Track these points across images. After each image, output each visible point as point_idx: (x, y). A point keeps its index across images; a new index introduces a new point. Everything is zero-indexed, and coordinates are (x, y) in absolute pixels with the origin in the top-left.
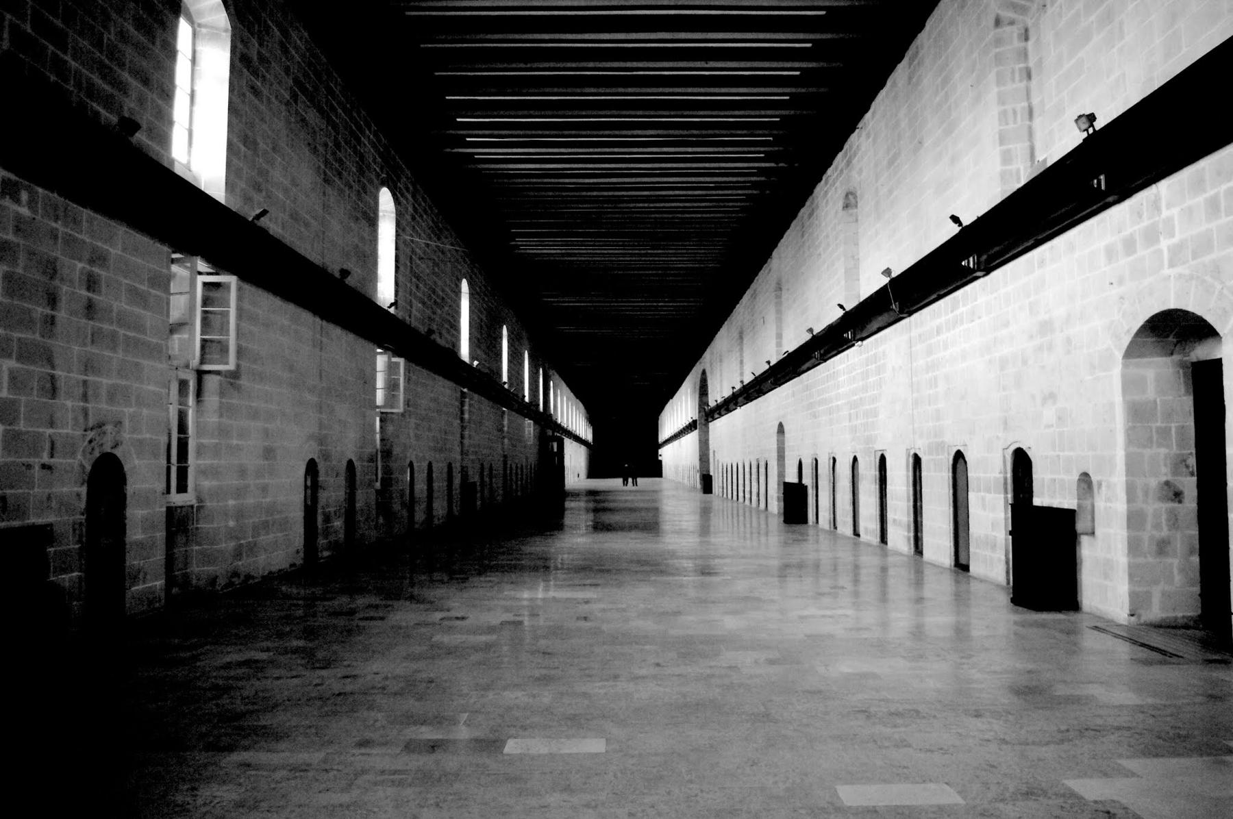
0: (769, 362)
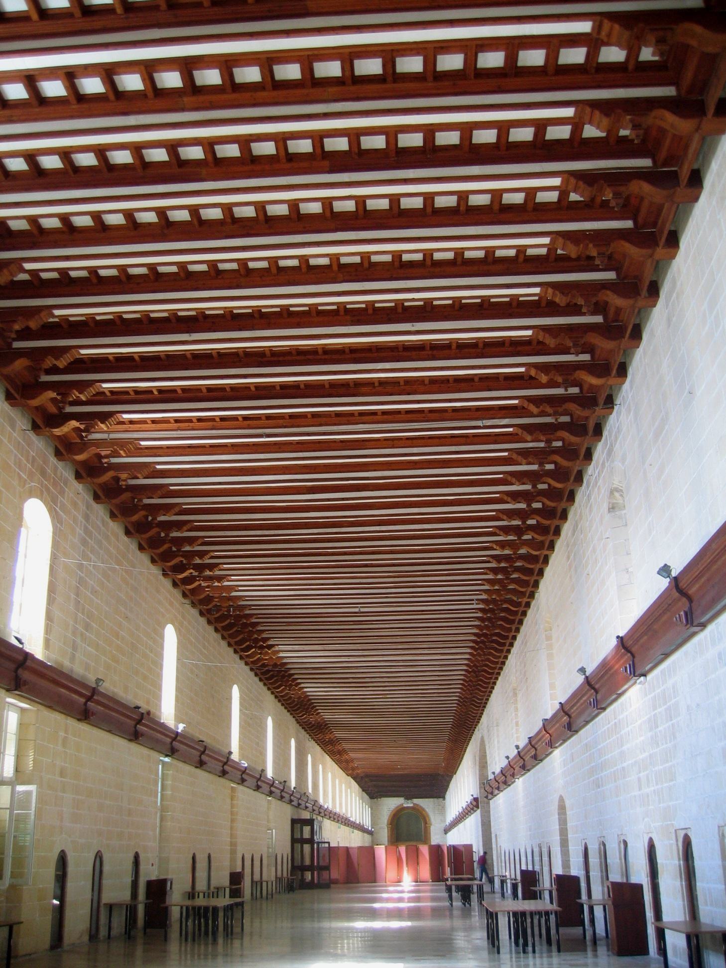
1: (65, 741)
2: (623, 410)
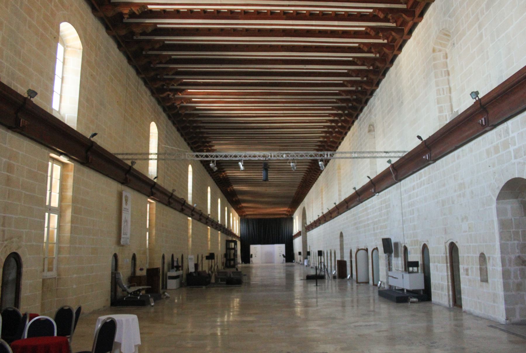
0: (335, 204)
2: (377, 98)
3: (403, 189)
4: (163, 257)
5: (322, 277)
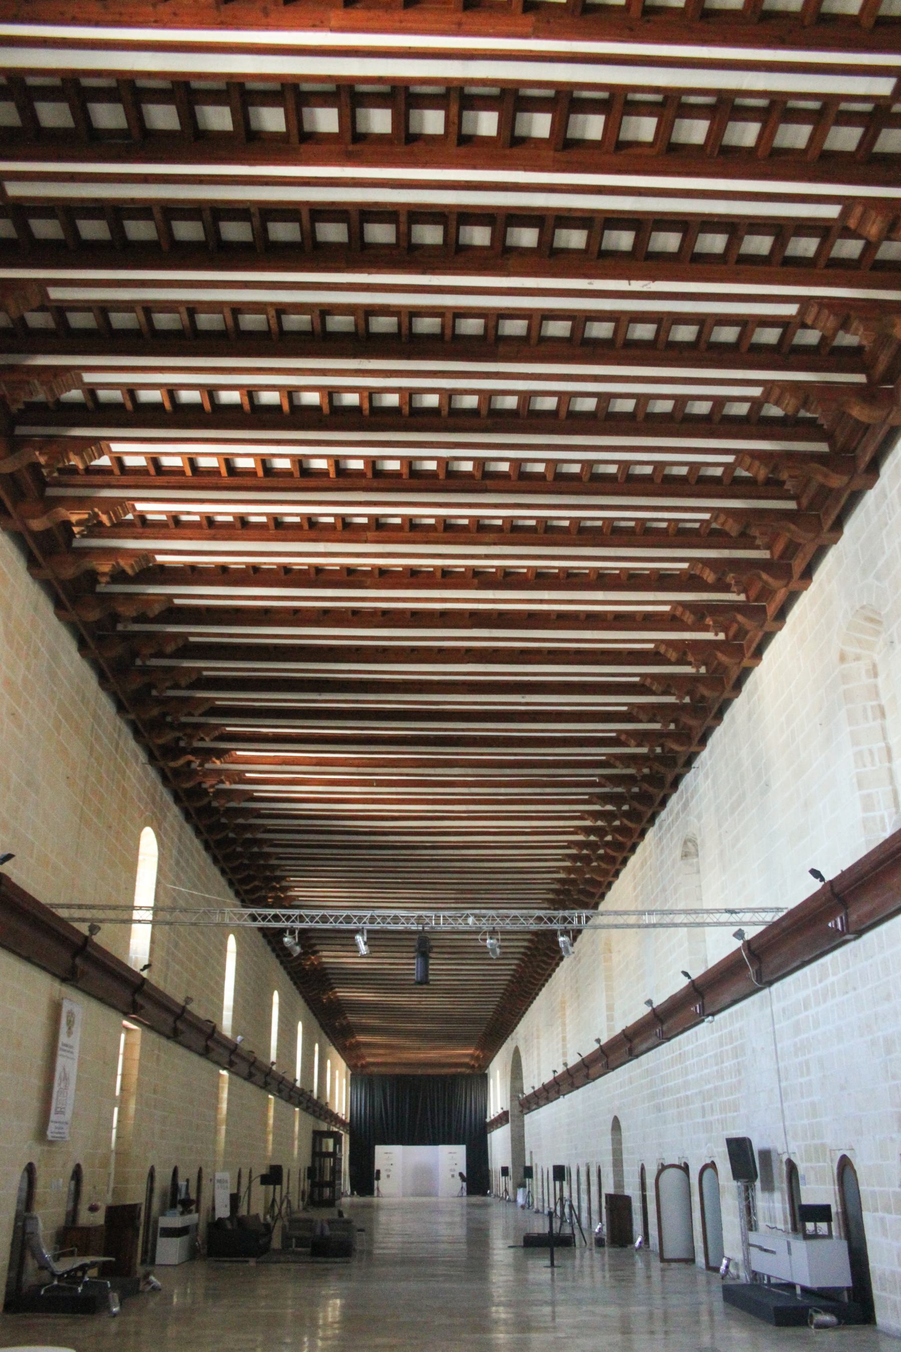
0: (598, 1041)
1: (158, 1059)
2: (701, 775)
3: (777, 1006)
4: (151, 1176)
5: (566, 1242)
